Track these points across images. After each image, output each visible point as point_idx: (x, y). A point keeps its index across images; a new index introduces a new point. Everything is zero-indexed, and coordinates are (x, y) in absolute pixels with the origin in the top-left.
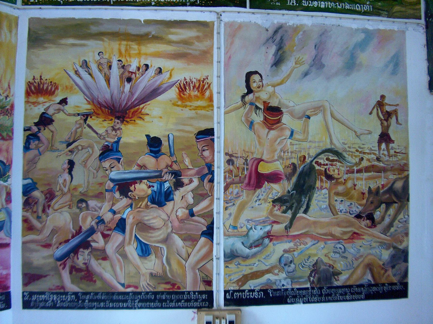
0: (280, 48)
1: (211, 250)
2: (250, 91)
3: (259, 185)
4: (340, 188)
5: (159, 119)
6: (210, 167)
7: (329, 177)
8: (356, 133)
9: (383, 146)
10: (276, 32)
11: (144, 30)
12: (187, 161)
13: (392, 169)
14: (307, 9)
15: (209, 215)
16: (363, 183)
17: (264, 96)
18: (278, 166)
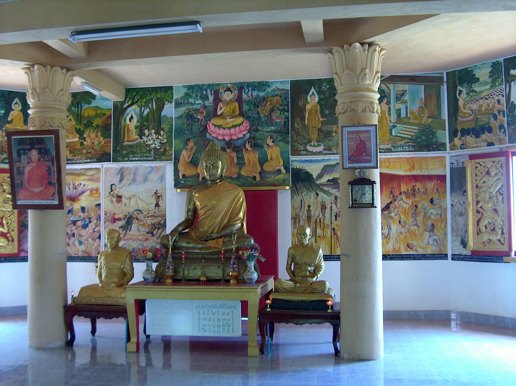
0: (122, 175)
1: (100, 244)
2: (112, 191)
3: (114, 222)
4: (141, 223)
5: (84, 201)
6: (100, 216)
7: (138, 219)
8: (146, 203)
9: (157, 208)
10: (120, 170)
11: (79, 172)
12: (93, 214)
13: (160, 216)
15: (99, 232)
16: (149, 221)
17: (116, 192)
18: (121, 216)
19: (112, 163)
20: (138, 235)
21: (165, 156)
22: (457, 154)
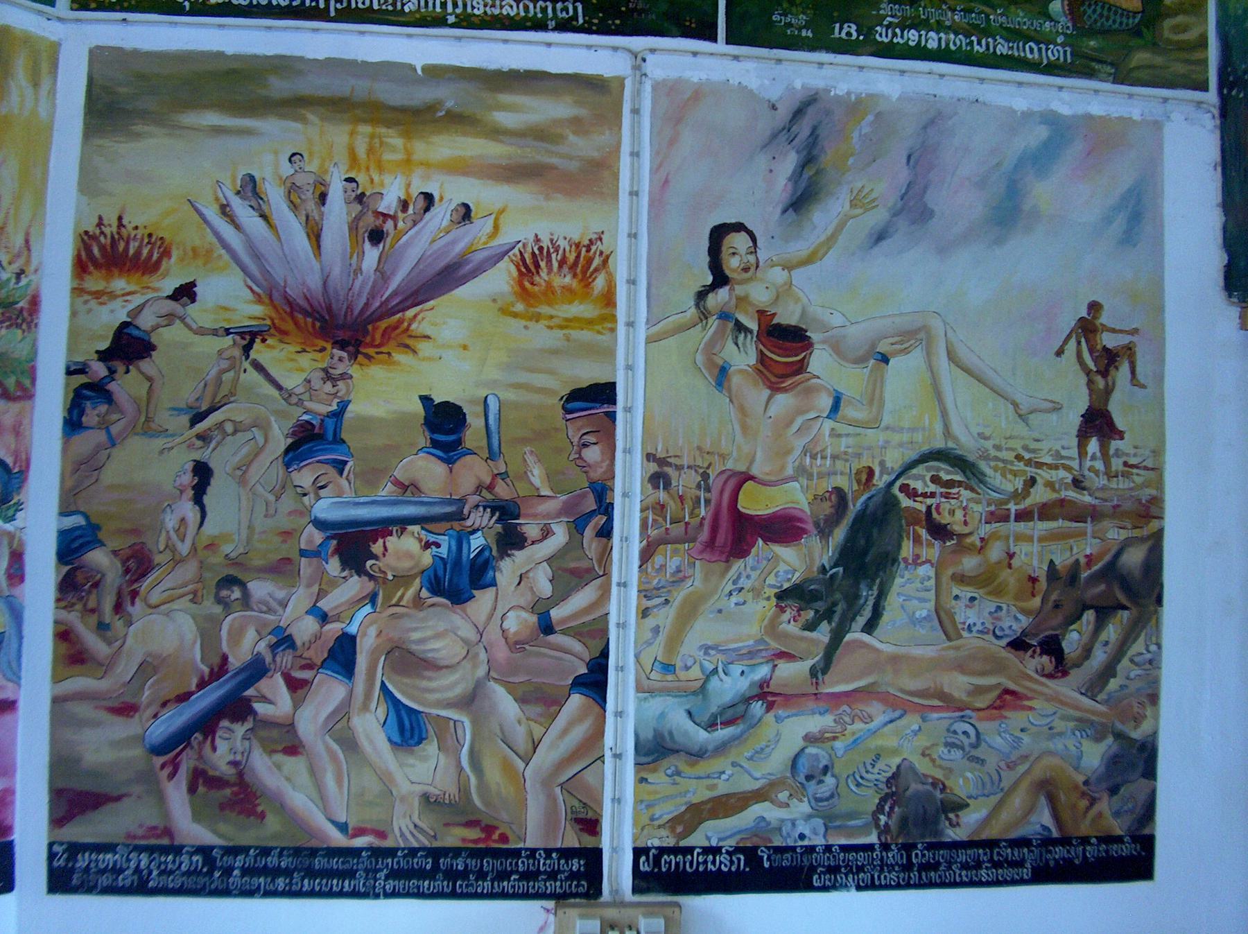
0: (808, 160)
1: (599, 733)
2: (720, 279)
4: (969, 563)
5: (458, 351)
7: (940, 532)
8: (1015, 407)
9: (1093, 446)
10: (798, 113)
11: (423, 95)
12: (537, 476)
14: (888, 51)
15: (595, 632)
16: (1034, 550)
17: (760, 294)
18: (795, 497)
19: (721, 46)
20: (937, 664)
21: (1154, 46)
22: (522, 380)
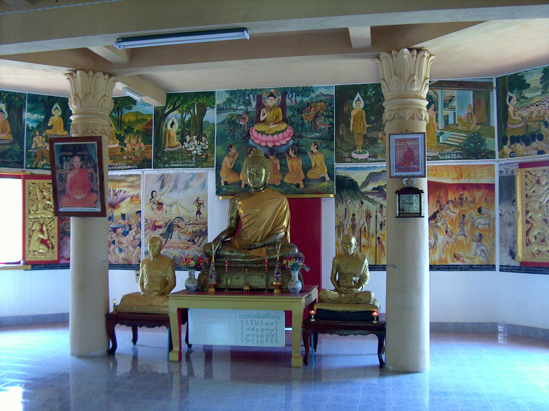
0: (163, 182)
2: (153, 198)
3: (155, 229)
4: (182, 231)
6: (140, 223)
7: (179, 227)
8: (187, 210)
11: (120, 178)
12: (133, 222)
13: (201, 224)
14: (172, 167)
15: (140, 239)
16: (191, 229)
17: (157, 199)
18: (161, 223)
20: (178, 243)
21: (207, 162)
